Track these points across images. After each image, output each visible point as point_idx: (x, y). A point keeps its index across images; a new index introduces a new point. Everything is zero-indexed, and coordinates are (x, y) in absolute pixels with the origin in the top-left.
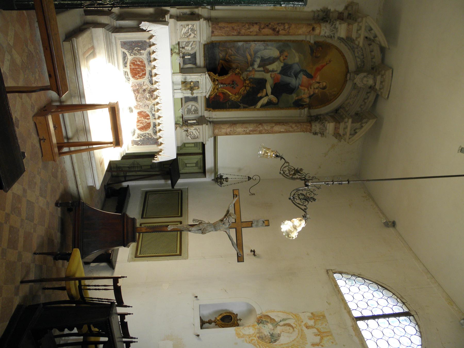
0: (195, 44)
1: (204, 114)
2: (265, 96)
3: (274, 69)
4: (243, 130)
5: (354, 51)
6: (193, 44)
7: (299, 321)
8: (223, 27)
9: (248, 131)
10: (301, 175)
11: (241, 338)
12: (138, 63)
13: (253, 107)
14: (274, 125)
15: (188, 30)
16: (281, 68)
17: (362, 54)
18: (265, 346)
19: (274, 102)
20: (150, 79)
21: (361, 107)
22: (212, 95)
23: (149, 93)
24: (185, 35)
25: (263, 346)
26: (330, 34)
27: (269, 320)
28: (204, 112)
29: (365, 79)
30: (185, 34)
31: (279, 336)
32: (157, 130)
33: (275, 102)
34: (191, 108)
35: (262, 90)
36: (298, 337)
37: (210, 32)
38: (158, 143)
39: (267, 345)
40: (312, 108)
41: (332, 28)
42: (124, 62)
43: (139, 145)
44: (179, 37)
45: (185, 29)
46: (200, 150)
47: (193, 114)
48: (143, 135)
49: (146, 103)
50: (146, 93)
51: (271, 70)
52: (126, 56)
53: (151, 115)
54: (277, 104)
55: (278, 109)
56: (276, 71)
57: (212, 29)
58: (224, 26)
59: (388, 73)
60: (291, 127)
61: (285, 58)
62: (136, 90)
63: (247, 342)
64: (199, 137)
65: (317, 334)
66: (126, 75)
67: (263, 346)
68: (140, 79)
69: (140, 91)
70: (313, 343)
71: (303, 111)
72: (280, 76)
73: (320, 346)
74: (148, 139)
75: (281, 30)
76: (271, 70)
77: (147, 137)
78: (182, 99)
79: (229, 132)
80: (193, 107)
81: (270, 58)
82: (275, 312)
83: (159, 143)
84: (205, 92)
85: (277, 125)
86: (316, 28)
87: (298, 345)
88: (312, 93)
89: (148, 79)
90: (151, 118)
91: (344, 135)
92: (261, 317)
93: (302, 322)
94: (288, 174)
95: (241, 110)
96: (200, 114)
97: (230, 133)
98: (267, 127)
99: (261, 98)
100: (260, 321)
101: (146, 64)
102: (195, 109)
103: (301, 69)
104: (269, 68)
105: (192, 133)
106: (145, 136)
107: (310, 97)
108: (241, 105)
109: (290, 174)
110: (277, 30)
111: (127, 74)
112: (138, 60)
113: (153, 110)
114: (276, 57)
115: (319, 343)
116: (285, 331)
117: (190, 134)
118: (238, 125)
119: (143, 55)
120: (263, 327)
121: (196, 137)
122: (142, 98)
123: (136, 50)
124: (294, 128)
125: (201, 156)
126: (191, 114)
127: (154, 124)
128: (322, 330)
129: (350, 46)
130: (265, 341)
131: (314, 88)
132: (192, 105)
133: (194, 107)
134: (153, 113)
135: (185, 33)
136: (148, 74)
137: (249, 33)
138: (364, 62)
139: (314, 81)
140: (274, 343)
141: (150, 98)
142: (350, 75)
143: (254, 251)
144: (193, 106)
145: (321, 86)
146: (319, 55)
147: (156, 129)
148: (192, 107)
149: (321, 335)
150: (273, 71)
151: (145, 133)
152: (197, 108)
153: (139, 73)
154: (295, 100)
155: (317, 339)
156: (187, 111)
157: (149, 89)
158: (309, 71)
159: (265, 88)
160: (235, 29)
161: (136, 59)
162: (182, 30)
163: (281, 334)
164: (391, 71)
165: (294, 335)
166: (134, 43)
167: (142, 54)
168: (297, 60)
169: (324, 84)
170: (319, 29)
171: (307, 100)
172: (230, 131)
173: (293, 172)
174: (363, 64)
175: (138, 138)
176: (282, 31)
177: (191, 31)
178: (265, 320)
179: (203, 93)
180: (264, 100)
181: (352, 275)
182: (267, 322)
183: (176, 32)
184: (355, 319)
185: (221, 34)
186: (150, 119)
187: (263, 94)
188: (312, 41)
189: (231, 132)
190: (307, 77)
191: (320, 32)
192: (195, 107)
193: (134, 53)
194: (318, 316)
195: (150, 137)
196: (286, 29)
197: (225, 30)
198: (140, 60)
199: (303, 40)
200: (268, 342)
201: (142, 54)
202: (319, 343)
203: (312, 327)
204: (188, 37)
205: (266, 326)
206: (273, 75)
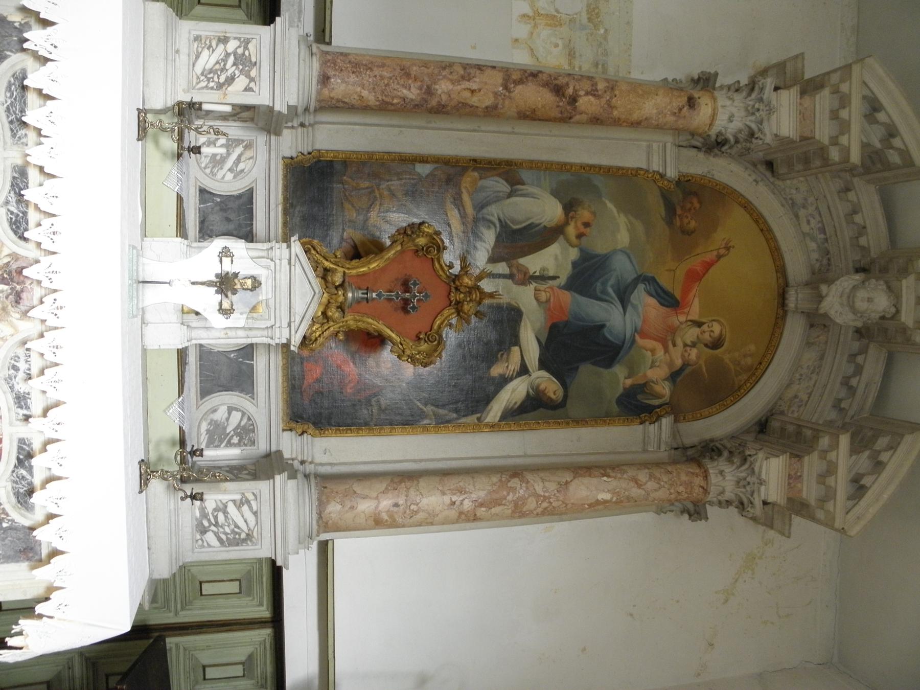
0: (252, 158)
1: (278, 443)
3: (548, 270)
4: (447, 499)
5: (797, 216)
6: (243, 158)
9: (467, 505)
13: (472, 419)
14: (568, 476)
15: (225, 60)
16: (570, 267)
19: (550, 398)
20: (15, 211)
21: (843, 405)
22: (316, 339)
24: (208, 80)
28: (278, 437)
29: (861, 294)
30: (207, 74)
32: (37, 481)
34: (228, 419)
35: (508, 350)
37: (315, 73)
38: (36, 553)
40: (684, 419)
41: (751, 103)
44: (182, 83)
45: (210, 56)
46: (264, 608)
51: (535, 272)
54: (562, 404)
55: (568, 423)
56: (554, 278)
57: (321, 65)
60: (636, 481)
61: (582, 229)
64: (255, 534)
71: (652, 429)
72: (567, 297)
75: (582, 93)
76: (537, 274)
80: (236, 417)
81: (531, 226)
83: (44, 552)
84: (285, 324)
85: (581, 476)
86: (699, 100)
88: (679, 363)
91: (822, 501)
96: (262, 447)
97: (391, 516)
98: (544, 487)
99: (504, 381)
102: (243, 423)
103: (639, 273)
105: (226, 517)
107: (674, 376)
110: (570, 91)
113: (21, 375)
114: (553, 224)
117: (217, 522)
118: (423, 483)
121: (243, 536)
124: (645, 484)
125: (266, 633)
127: (20, 448)
131: (685, 345)
132: (230, 410)
133: (240, 414)
134: (17, 387)
135: (211, 71)
137: (467, 94)
138: (828, 253)
139: (682, 318)
144: (234, 413)
145: (707, 336)
146: (693, 224)
147: (28, 477)
148: (229, 414)
150: (542, 278)
152: (249, 419)
154: (625, 389)
156: (208, 431)
157: (6, 260)
158: (665, 281)
159: (516, 341)
160: (413, 73)
162: (198, 56)
168: (623, 238)
169: (717, 328)
170: (710, 105)
171: (665, 389)
172: (392, 509)
174: (825, 262)
176: (586, 99)
177: (234, 64)
179: (277, 330)
183: (170, 58)
185: (359, 89)
187: (511, 367)
189: (395, 509)
190: (661, 304)
191: (714, 114)
192: (244, 414)
196: (600, 93)
197: (375, 76)
199: (641, 169)
204: (220, 86)
206: (545, 291)
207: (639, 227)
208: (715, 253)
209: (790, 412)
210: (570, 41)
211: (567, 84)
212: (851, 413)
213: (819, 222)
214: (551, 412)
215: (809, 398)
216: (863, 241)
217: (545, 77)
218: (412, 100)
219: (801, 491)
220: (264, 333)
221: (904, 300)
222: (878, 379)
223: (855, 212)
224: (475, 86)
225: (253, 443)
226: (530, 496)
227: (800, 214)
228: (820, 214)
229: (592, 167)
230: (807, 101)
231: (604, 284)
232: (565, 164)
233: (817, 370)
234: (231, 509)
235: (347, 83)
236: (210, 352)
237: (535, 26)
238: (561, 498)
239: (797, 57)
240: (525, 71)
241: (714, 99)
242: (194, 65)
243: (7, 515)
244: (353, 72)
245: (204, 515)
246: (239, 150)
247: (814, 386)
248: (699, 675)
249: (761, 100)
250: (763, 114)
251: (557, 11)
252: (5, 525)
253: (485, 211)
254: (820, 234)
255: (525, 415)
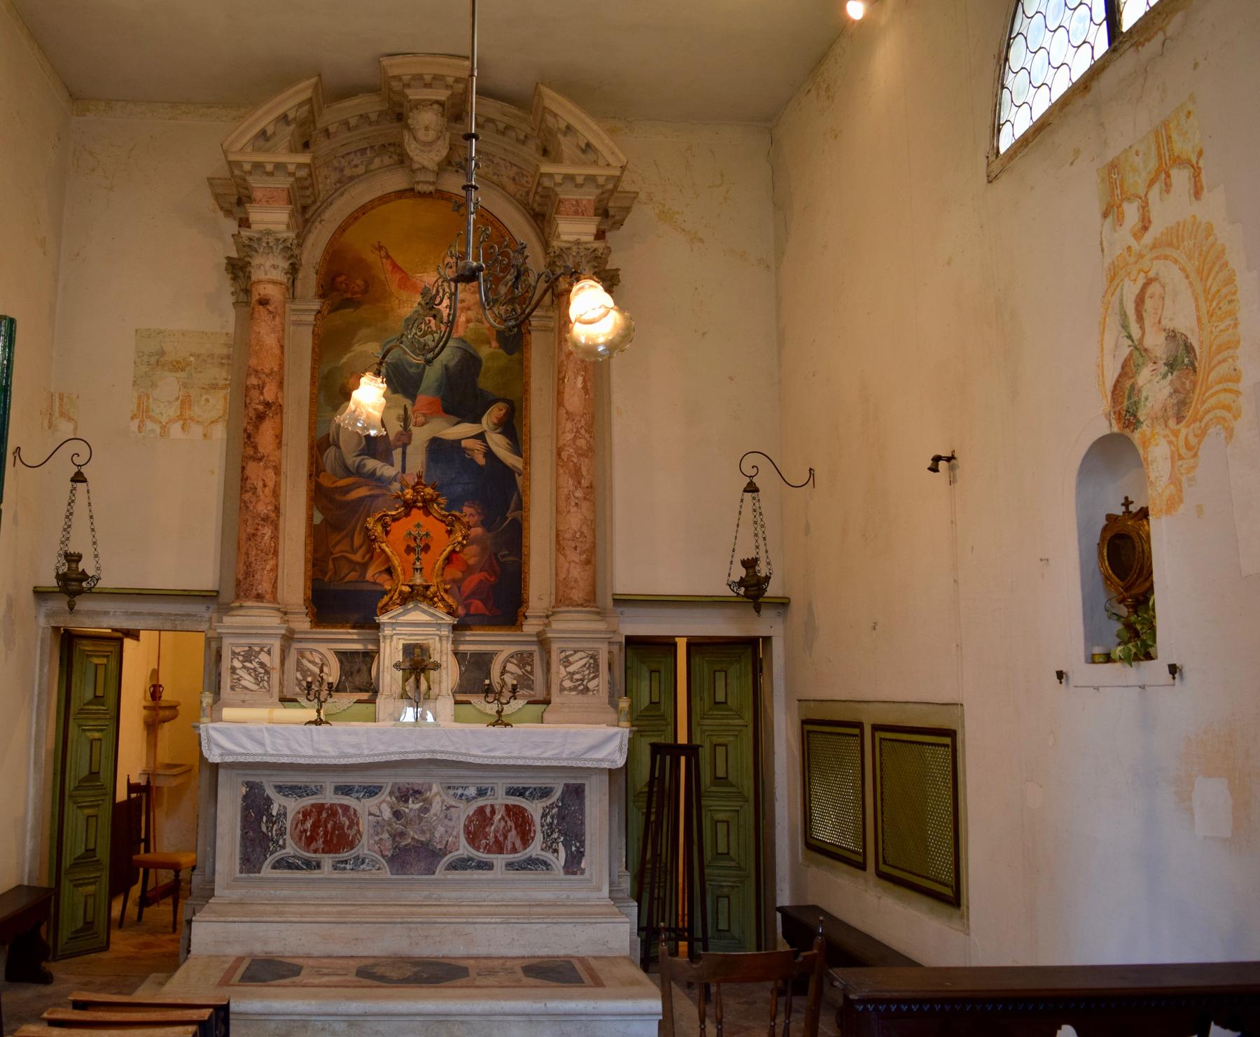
2: (485, 441)
3: (399, 415)
4: (573, 509)
5: (351, 178)
7: (1127, 264)
8: (247, 567)
10: (441, 294)
11: (1181, 491)
12: (308, 825)
13: (519, 479)
15: (248, 669)
16: (397, 396)
17: (358, 154)
18: (1204, 389)
19: (504, 415)
21: (522, 138)
23: (406, 801)
25: (1204, 398)
26: (279, 254)
27: (1128, 384)
28: (525, 635)
29: (421, 135)
31: (1172, 336)
33: (504, 411)
34: (512, 673)
35: (464, 450)
36: (1176, 256)
39: (1202, 381)
42: (303, 869)
43: (582, 850)
47: (532, 669)
48: (547, 833)
49: (438, 813)
50: (407, 810)
52: (288, 862)
53: (481, 802)
54: (510, 403)
55: (527, 399)
58: (245, 563)
59: (396, 68)
62: (394, 839)
63: (1194, 467)
64: (591, 653)
65: (1166, 184)
66: (345, 869)
67: (1204, 398)
68: (360, 826)
69: (398, 830)
70: (1192, 191)
72: (422, 398)
73: (1201, 164)
74: (563, 818)
75: (262, 398)
76: (402, 424)
77: (555, 822)
78: (457, 703)
79: (580, 554)
82: (1103, 361)
87: (1200, 254)
89: (362, 800)
90: (489, 802)
92: (1120, 413)
93: (1129, 248)
94: (437, 336)
95: (528, 516)
99: (489, 454)
100: (1131, 418)
101: (313, 802)
102: (516, 662)
104: (396, 432)
105: (578, 673)
106: (551, 827)
108: (510, 516)
109: (434, 329)
110: (261, 407)
111: (343, 866)
112: (299, 825)
115: (1192, 166)
116: (1159, 314)
117: (581, 680)
119: (284, 807)
120: (1147, 403)
121: (592, 661)
122: (422, 824)
123: (267, 828)
126: (533, 675)
128: (1153, 164)
129: (335, 191)
130: (1189, 391)
134: (474, 795)
136: (348, 797)
138: (383, 145)
140: (1195, 355)
141: (424, 801)
142: (418, 183)
143: (937, 459)
146: (359, 282)
149: (1169, 165)
150: (406, 420)
151: (542, 826)
153: (341, 827)
154: (500, 347)
155: (1181, 178)
157: (394, 799)
161: (298, 830)
162: (246, 688)
163: (1168, 328)
164: (386, 62)
165: (1171, 274)
166: (247, 833)
167: (282, 812)
173: (431, 318)
174: (392, 149)
175: (556, 851)
176: (266, 395)
177: (251, 662)
178: (1126, 400)
180: (498, 444)
181: (1003, 87)
182: (1134, 389)
184: (1116, 44)
186: (492, 806)
187: (478, 447)
188: (316, 305)
189: (578, 549)
193: (277, 835)
194: (1113, 189)
195: (555, 810)
198: (301, 818)
200: (1192, 378)
201: (282, 812)
202: (1192, 166)
203: (1144, 207)
204: (267, 672)
205: (1144, 394)
207: (365, 332)
208: (384, 260)
209: (526, 185)
210: (202, 388)
211: (255, 409)
212: (529, 130)
213: (356, 155)
214: (517, 413)
215: (515, 165)
216: (373, 117)
217: (250, 428)
218: (272, 532)
219: (589, 200)
220: (444, 642)
221: (427, 97)
222: (499, 104)
223: (346, 123)
224: (261, 484)
225: (531, 654)
226: (575, 444)
227: (349, 175)
228: (348, 154)
229: (313, 376)
230: (258, 195)
231: (411, 365)
232: (311, 399)
233: (490, 157)
234: (571, 669)
235: (261, 581)
236: (460, 686)
237: (192, 419)
238: (578, 418)
239: (211, 184)
240: (245, 443)
241: (260, 282)
242: (252, 691)
243: (553, 803)
244: (253, 576)
245: (575, 689)
246: (305, 662)
247: (504, 160)
248: (768, 266)
249: (259, 239)
250: (271, 239)
251: (177, 399)
252: (560, 804)
253: (351, 469)
254: (366, 154)
255: (518, 436)
